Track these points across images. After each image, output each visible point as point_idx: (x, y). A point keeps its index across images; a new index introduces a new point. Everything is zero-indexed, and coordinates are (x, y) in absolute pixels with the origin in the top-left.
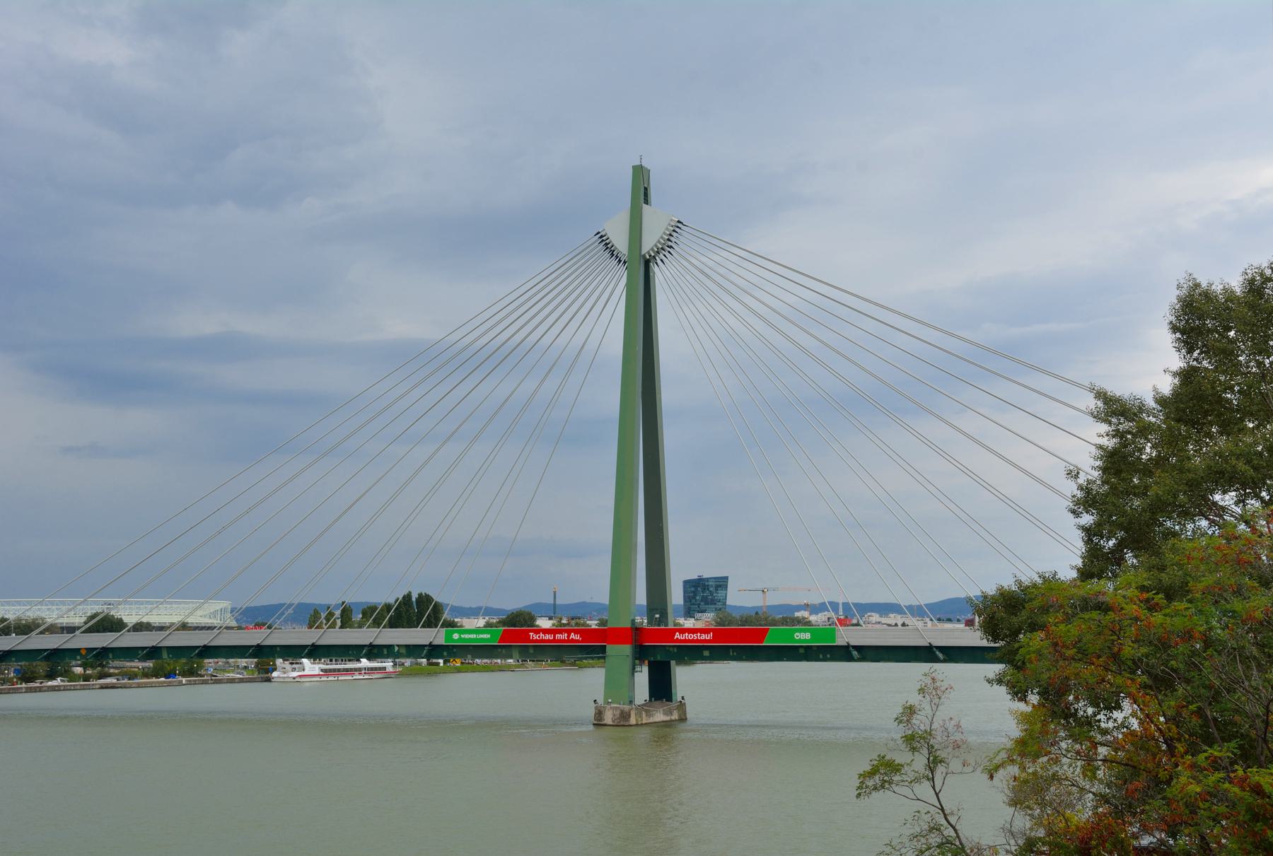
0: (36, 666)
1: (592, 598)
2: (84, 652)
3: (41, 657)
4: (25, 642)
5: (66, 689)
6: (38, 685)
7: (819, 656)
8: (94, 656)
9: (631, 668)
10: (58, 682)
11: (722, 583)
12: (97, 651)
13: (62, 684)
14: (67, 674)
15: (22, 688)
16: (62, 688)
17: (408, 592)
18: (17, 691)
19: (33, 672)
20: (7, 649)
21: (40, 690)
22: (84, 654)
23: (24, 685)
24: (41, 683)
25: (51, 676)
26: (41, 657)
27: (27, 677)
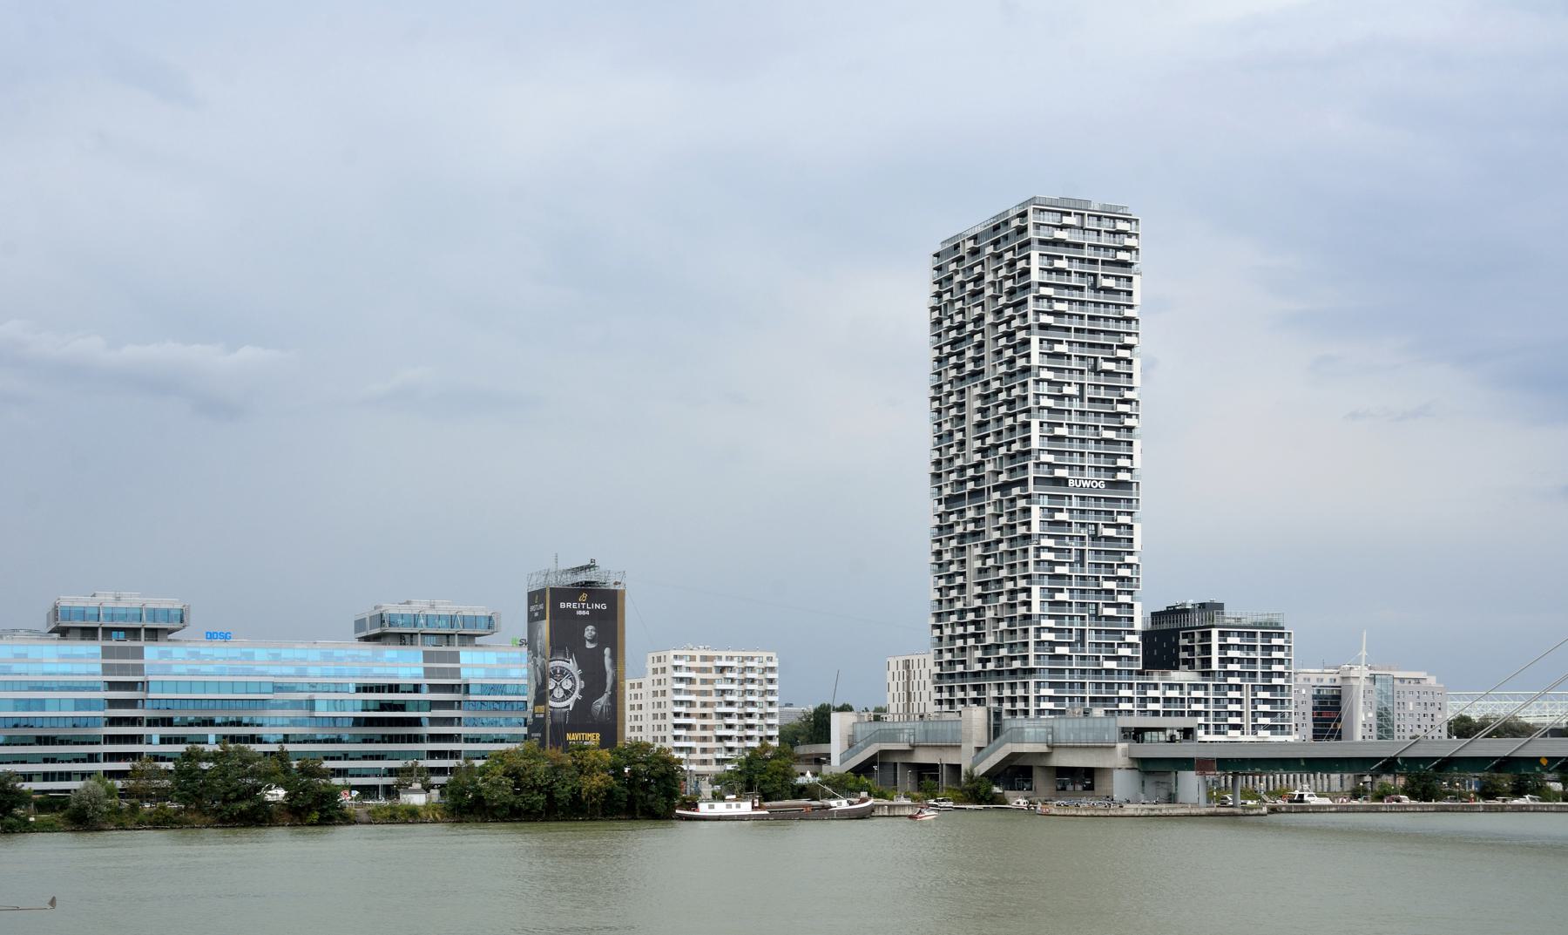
0: (1498, 778)
1: (433, 606)
2: (1544, 762)
3: (1554, 766)
4: (1468, 747)
5: (1536, 810)
6: (1500, 803)
7: (1419, 767)
8: (1558, 768)
9: (1141, 784)
10: (1526, 800)
11: (1220, 606)
12: (1562, 761)
13: (1533, 803)
14: (1541, 791)
15: (1479, 806)
16: (1532, 809)
17: (481, 611)
18: (1472, 809)
19: (1494, 787)
20: (1447, 756)
21: (1502, 809)
22: (1545, 764)
23: (1482, 803)
24: (1504, 800)
25: (1519, 792)
26: (1554, 766)
27: (1487, 793)
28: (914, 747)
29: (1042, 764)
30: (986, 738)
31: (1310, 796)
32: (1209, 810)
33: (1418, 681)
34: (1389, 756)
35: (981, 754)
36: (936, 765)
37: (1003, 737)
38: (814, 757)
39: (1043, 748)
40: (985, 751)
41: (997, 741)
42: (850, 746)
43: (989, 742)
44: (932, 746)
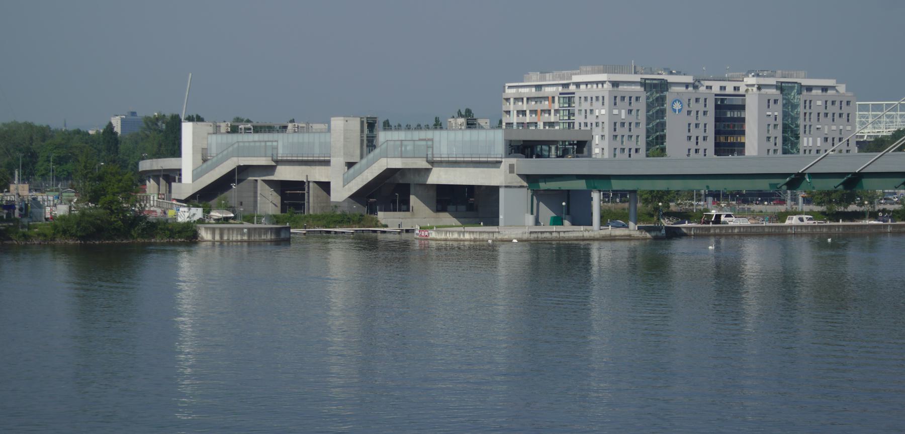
28: (433, 163)
29: (421, 182)
30: (358, 152)
31: (727, 216)
32: (603, 233)
33: (825, 89)
34: (796, 172)
35: (352, 170)
36: (302, 183)
37: (377, 151)
38: (162, 173)
39: (422, 164)
40: (356, 167)
41: (371, 155)
42: (205, 160)
43: (362, 157)
44: (472, 162)
